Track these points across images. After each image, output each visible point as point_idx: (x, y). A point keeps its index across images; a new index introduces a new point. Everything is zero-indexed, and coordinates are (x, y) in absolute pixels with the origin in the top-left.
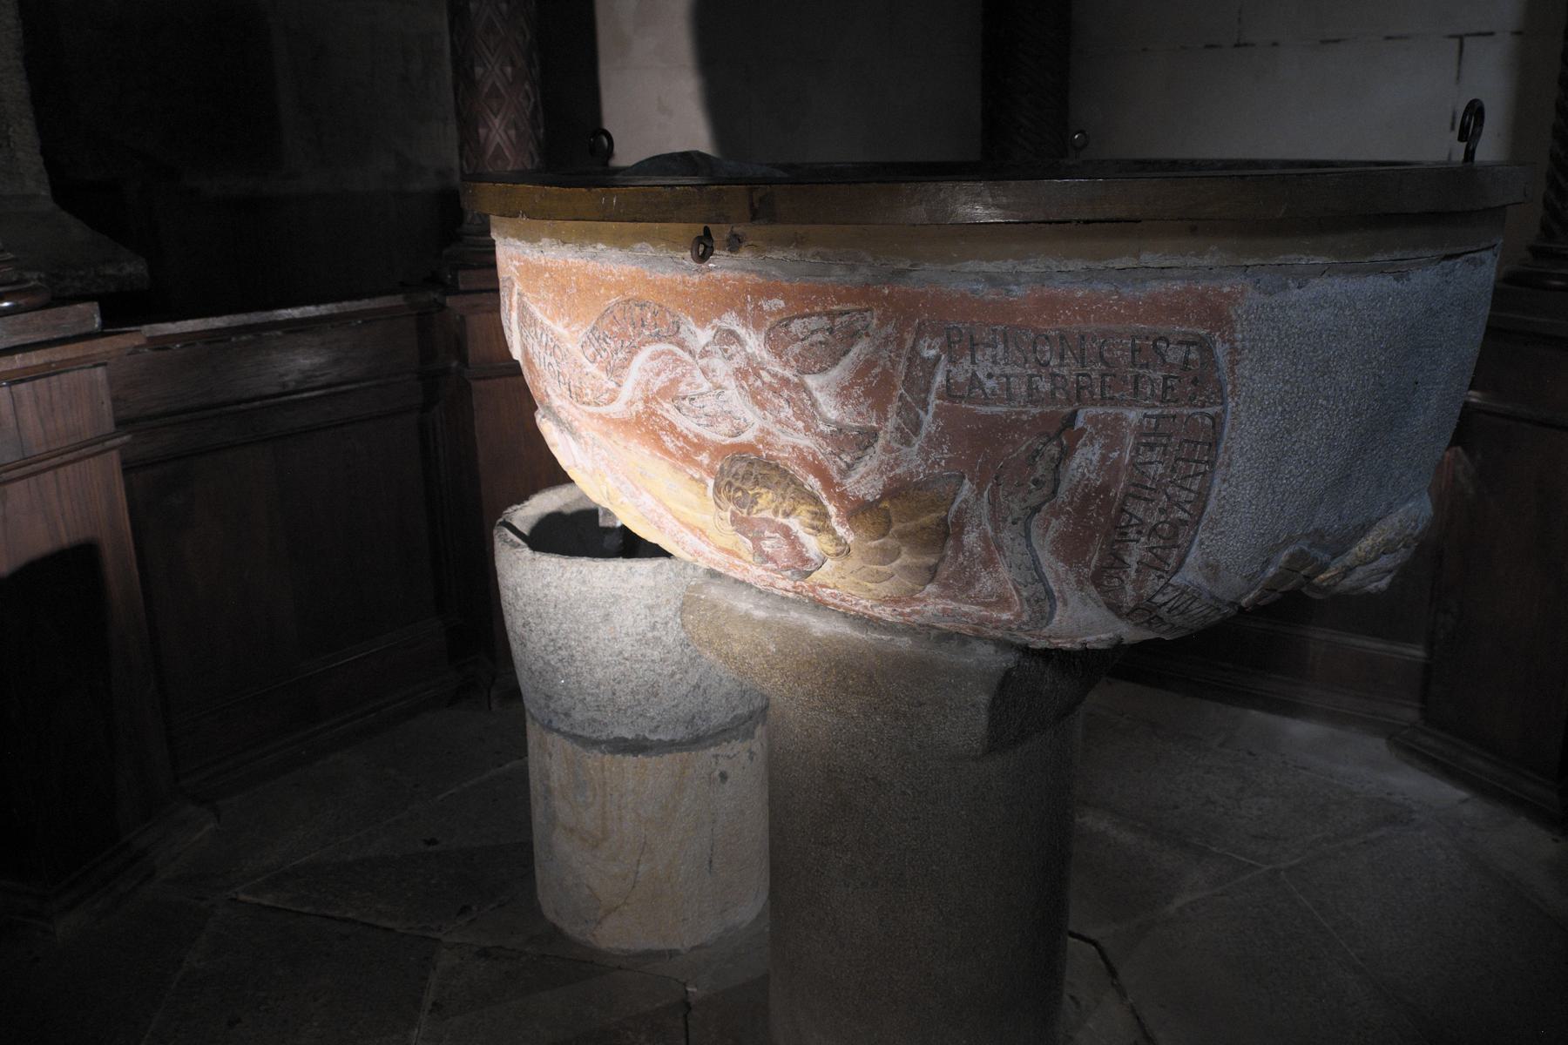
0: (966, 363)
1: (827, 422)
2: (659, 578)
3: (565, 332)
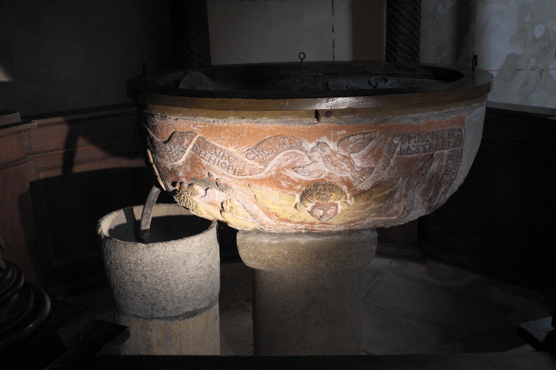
0: (407, 144)
1: (358, 167)
2: (202, 242)
3: (235, 150)
